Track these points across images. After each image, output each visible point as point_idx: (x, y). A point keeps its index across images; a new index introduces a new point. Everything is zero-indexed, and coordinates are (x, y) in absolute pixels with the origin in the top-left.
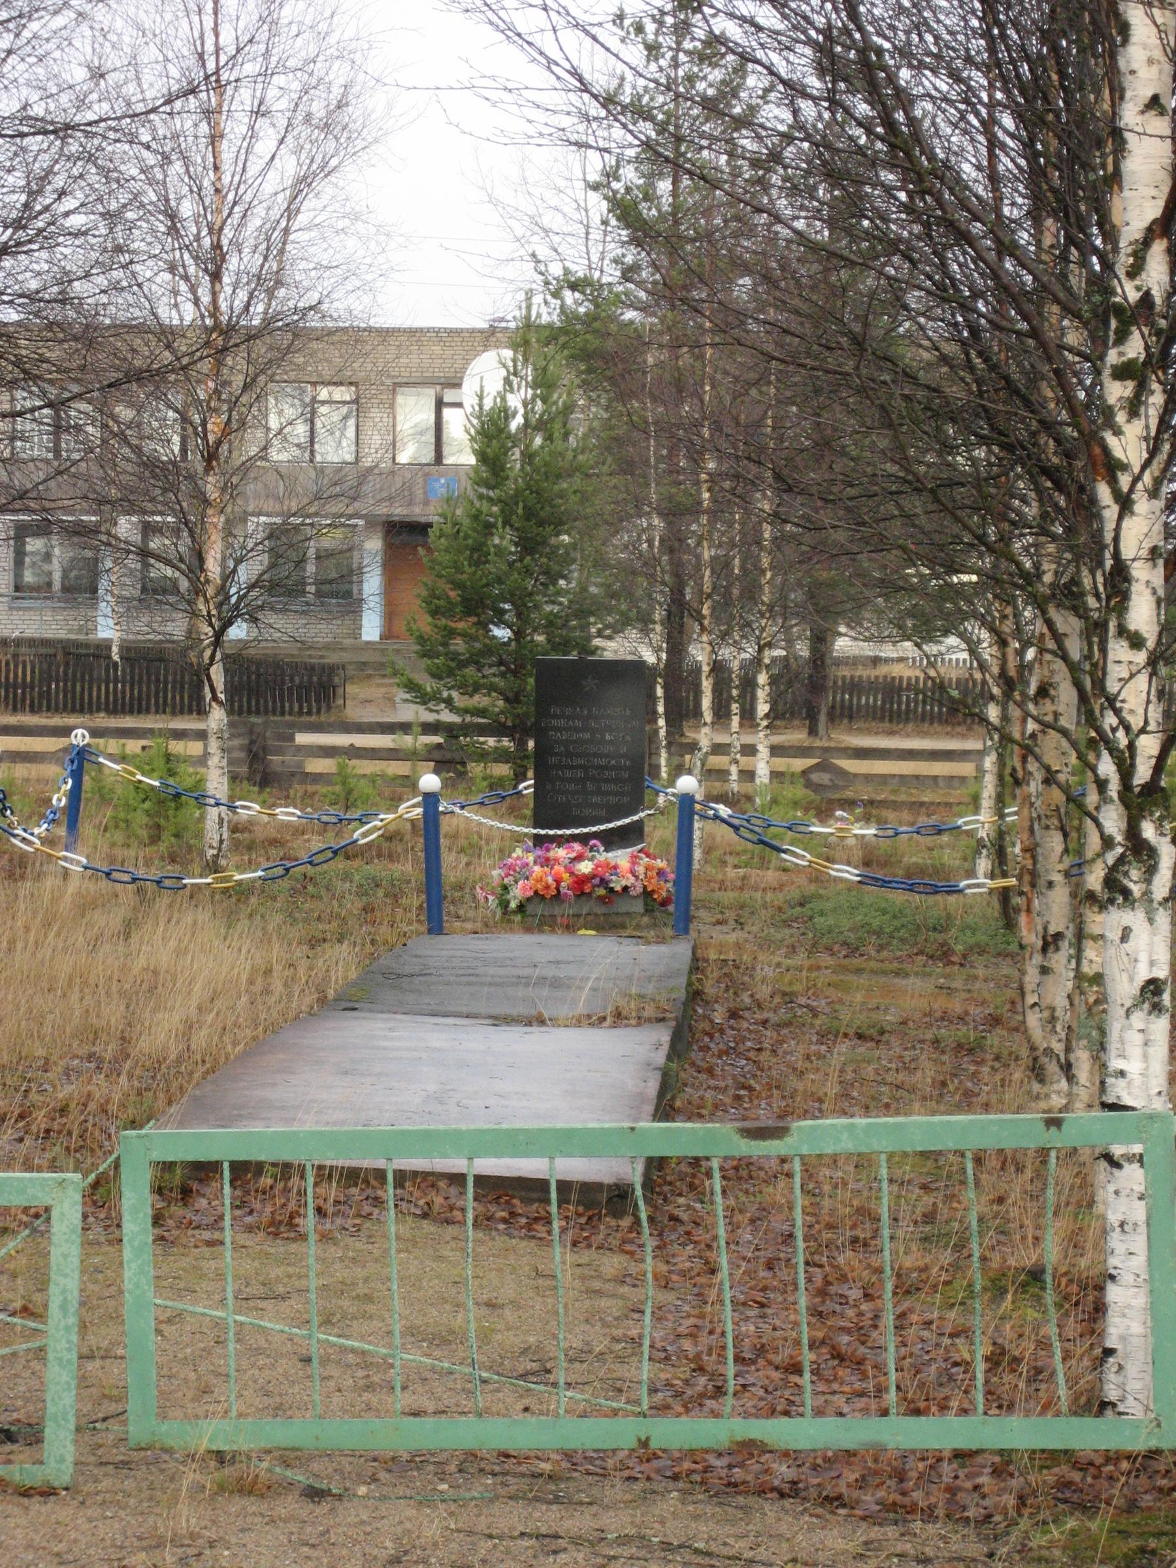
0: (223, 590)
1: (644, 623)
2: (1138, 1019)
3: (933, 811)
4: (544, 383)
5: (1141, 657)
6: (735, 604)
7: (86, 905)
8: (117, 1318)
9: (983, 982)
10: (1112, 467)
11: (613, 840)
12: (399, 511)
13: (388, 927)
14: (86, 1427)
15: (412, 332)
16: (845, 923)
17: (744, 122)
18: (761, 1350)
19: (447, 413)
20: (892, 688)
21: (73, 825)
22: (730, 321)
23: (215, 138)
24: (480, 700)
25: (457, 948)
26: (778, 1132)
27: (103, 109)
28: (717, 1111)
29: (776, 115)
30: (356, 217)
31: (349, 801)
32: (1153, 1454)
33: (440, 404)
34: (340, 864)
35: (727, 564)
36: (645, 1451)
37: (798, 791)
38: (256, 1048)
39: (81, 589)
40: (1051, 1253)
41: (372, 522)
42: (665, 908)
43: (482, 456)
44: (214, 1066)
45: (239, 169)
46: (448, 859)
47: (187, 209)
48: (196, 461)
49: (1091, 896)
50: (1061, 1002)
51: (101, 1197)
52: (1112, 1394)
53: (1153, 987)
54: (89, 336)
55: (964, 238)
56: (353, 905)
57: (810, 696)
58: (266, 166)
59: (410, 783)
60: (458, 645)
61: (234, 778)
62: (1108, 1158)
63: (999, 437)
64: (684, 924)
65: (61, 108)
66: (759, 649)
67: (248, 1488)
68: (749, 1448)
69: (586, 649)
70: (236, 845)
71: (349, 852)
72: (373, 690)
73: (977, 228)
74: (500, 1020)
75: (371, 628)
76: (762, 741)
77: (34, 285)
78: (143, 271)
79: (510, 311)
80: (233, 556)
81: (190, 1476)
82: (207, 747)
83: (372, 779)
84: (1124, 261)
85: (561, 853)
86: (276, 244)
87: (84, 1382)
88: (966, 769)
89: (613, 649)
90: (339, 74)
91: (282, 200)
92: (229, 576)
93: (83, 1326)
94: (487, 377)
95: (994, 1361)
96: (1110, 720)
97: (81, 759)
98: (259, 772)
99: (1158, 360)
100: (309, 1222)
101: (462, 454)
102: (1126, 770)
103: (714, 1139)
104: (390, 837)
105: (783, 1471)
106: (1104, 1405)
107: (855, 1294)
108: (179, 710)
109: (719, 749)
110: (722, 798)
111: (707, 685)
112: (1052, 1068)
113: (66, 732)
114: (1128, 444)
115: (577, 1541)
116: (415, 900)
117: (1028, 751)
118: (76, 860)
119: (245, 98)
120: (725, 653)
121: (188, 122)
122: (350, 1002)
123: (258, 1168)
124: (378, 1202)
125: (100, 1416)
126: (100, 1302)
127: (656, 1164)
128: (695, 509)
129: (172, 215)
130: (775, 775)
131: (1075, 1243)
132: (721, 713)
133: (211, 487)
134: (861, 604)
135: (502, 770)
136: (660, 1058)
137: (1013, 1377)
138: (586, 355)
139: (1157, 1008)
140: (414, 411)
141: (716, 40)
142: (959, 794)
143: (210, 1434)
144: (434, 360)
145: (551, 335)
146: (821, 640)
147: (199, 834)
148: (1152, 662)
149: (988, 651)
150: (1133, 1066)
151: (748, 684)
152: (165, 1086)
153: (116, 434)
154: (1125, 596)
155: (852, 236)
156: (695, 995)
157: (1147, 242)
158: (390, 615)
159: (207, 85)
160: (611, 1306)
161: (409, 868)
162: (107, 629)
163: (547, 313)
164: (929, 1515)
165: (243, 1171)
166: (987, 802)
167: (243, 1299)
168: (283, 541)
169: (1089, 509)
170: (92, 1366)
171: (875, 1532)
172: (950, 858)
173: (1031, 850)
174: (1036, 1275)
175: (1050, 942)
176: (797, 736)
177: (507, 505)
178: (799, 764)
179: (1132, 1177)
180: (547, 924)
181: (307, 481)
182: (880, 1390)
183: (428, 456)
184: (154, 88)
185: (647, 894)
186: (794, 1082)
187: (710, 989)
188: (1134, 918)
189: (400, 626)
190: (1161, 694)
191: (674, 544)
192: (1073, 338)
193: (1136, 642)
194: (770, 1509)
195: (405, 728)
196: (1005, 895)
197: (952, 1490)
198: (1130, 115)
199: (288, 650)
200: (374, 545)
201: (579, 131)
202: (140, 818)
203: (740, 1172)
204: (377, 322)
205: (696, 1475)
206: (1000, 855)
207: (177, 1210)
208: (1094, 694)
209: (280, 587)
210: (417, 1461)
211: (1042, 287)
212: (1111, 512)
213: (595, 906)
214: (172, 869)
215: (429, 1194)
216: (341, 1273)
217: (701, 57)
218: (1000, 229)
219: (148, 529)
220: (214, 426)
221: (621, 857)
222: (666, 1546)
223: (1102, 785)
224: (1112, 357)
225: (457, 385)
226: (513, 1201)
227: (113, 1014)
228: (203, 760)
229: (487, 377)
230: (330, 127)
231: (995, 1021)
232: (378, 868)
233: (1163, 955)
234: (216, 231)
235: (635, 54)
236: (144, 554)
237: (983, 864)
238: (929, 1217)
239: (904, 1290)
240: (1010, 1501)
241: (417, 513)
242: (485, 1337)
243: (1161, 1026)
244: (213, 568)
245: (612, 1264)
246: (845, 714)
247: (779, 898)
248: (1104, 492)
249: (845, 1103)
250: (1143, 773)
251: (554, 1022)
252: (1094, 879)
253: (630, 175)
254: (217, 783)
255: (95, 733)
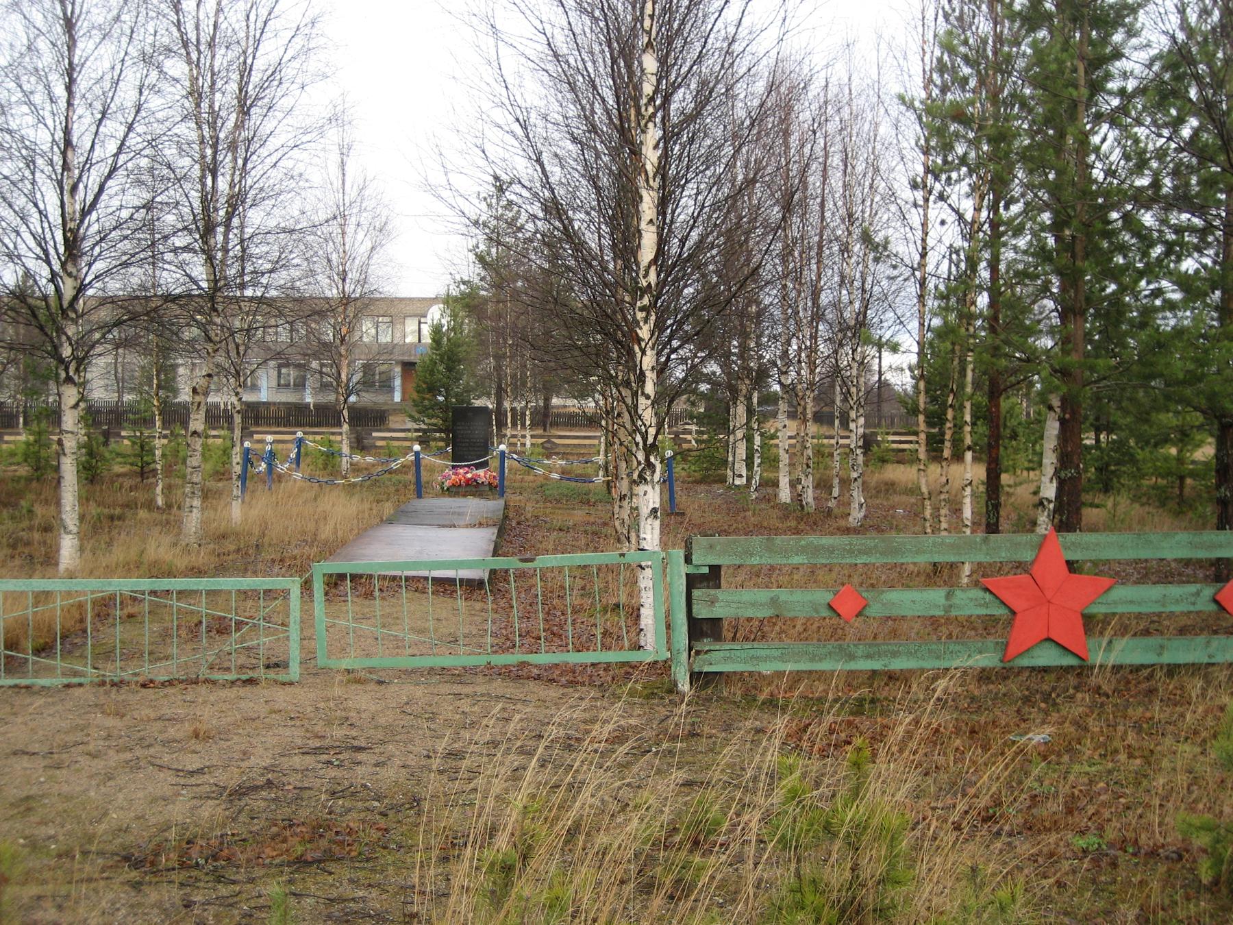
0: (347, 385)
1: (488, 395)
2: (650, 521)
3: (584, 455)
4: (454, 316)
5: (649, 402)
6: (519, 389)
7: (301, 490)
8: (313, 626)
9: (602, 510)
10: (639, 340)
11: (478, 466)
12: (406, 358)
13: (403, 495)
14: (303, 662)
15: (410, 299)
16: (555, 493)
17: (520, 229)
18: (528, 632)
19: (422, 326)
20: (571, 416)
21: (298, 464)
22: (516, 294)
23: (343, 233)
24: (434, 421)
25: (428, 503)
26: (532, 560)
27: (305, 224)
28: (513, 554)
29: (530, 226)
30: (391, 260)
31: (391, 455)
32: (656, 662)
33: (420, 323)
34: (387, 476)
35: (516, 375)
36: (489, 666)
37: (540, 450)
38: (359, 536)
39: (300, 385)
40: (623, 599)
41: (397, 363)
42: (496, 489)
43: (433, 340)
44: (344, 543)
45: (528, 13)
46: (423, 473)
47: (334, 257)
48: (338, 342)
49: (634, 481)
50: (626, 517)
51: (307, 586)
52: (642, 643)
53: (654, 510)
54: (300, 300)
55: (591, 266)
56: (392, 489)
57: (544, 418)
58: (359, 243)
59: (410, 449)
60: (426, 402)
61: (351, 448)
62: (640, 566)
63: (603, 331)
64: (502, 494)
65: (290, 224)
66: (529, 403)
67: (358, 681)
68: (523, 664)
69: (469, 403)
70: (354, 471)
71: (390, 472)
72: (399, 418)
73: (595, 263)
74: (440, 526)
75: (397, 397)
76: (528, 433)
77: (282, 282)
78: (319, 278)
79: (443, 292)
80: (351, 373)
81: (338, 678)
82: (342, 437)
83: (398, 448)
84: (642, 273)
85: (461, 471)
86: (364, 269)
87: (302, 648)
88: (596, 442)
89: (478, 403)
90: (385, 213)
91: (366, 255)
92: (349, 380)
93: (302, 630)
94: (435, 314)
95: (604, 634)
96: (640, 423)
97: (300, 442)
98: (360, 445)
99: (653, 305)
100: (377, 593)
101: (427, 339)
102: (645, 440)
103: (510, 563)
104: (403, 466)
105: (536, 671)
106: (640, 647)
107: (559, 613)
108: (333, 426)
109: (513, 436)
110: (515, 453)
111: (509, 415)
112: (623, 538)
113: (295, 433)
114: (644, 332)
115: (467, 696)
116: (412, 487)
117: (614, 435)
118: (297, 475)
119: (352, 221)
120: (515, 404)
121: (334, 228)
122: (390, 522)
123: (361, 576)
124: (400, 587)
125: (307, 659)
126: (307, 621)
127: (493, 572)
128: (504, 356)
129: (329, 261)
130: (608, 531)
131: (631, 595)
132: (514, 425)
133: (343, 350)
134: (560, 387)
135: (442, 444)
136: (494, 538)
137: (610, 639)
138: (467, 306)
139: (656, 517)
140: (411, 325)
141: (510, 203)
142: (594, 450)
143: (345, 664)
144: (418, 308)
145: (456, 299)
146: (547, 400)
147: (340, 466)
148: (653, 404)
149: (601, 403)
150: (648, 537)
151: (523, 415)
152: (330, 550)
153: (310, 332)
154: (644, 382)
155: (556, 268)
156: (506, 517)
157: (649, 267)
158: (404, 392)
159: (340, 217)
160: (478, 619)
161: (411, 477)
162: (309, 399)
163: (455, 292)
164: (583, 684)
165: (354, 577)
166: (602, 453)
167: (355, 620)
168: (368, 368)
169: (631, 353)
170: (305, 642)
171: (566, 690)
172: (590, 471)
173: (616, 467)
174: (617, 605)
175: (623, 498)
176: (540, 432)
177: (442, 356)
178: (540, 441)
179: (648, 572)
180: (457, 494)
181: (375, 349)
182: (567, 644)
183: (416, 340)
184: (322, 216)
185: (490, 484)
186: (539, 545)
187: (511, 516)
188: (648, 488)
189: (407, 396)
190: (656, 414)
191: (498, 368)
192: (627, 299)
193: (648, 397)
194: (531, 684)
195: (409, 430)
196: (608, 483)
197: (591, 676)
198: (643, 226)
199: (370, 405)
200: (398, 369)
201: (464, 230)
202: (320, 461)
203: (521, 575)
204: (399, 295)
205: (506, 673)
206: (606, 469)
207: (333, 591)
208: (634, 412)
209: (367, 384)
210: (414, 671)
211: (617, 282)
212: (639, 355)
213: (472, 488)
214: (331, 478)
215: (416, 584)
216: (388, 610)
217: (505, 208)
218: (602, 263)
219: (322, 365)
220: (344, 330)
221: (481, 472)
222: (497, 697)
223: (637, 445)
224: (639, 304)
225: (425, 316)
226: (444, 585)
227: (311, 526)
228: (341, 442)
229: (435, 314)
230: (382, 229)
231: (605, 524)
232: (400, 477)
233: (658, 500)
234: (344, 265)
235: (484, 206)
236: (321, 373)
237: (601, 473)
238: (583, 588)
239: (574, 612)
240: (609, 679)
241: (412, 359)
242: (436, 630)
243: (657, 523)
244: (344, 377)
245: (478, 605)
246: (555, 424)
247: (534, 485)
248: (636, 348)
249: (555, 551)
250: (650, 440)
251: (459, 526)
252: (635, 476)
253: (482, 247)
254: (346, 449)
255: (305, 433)
